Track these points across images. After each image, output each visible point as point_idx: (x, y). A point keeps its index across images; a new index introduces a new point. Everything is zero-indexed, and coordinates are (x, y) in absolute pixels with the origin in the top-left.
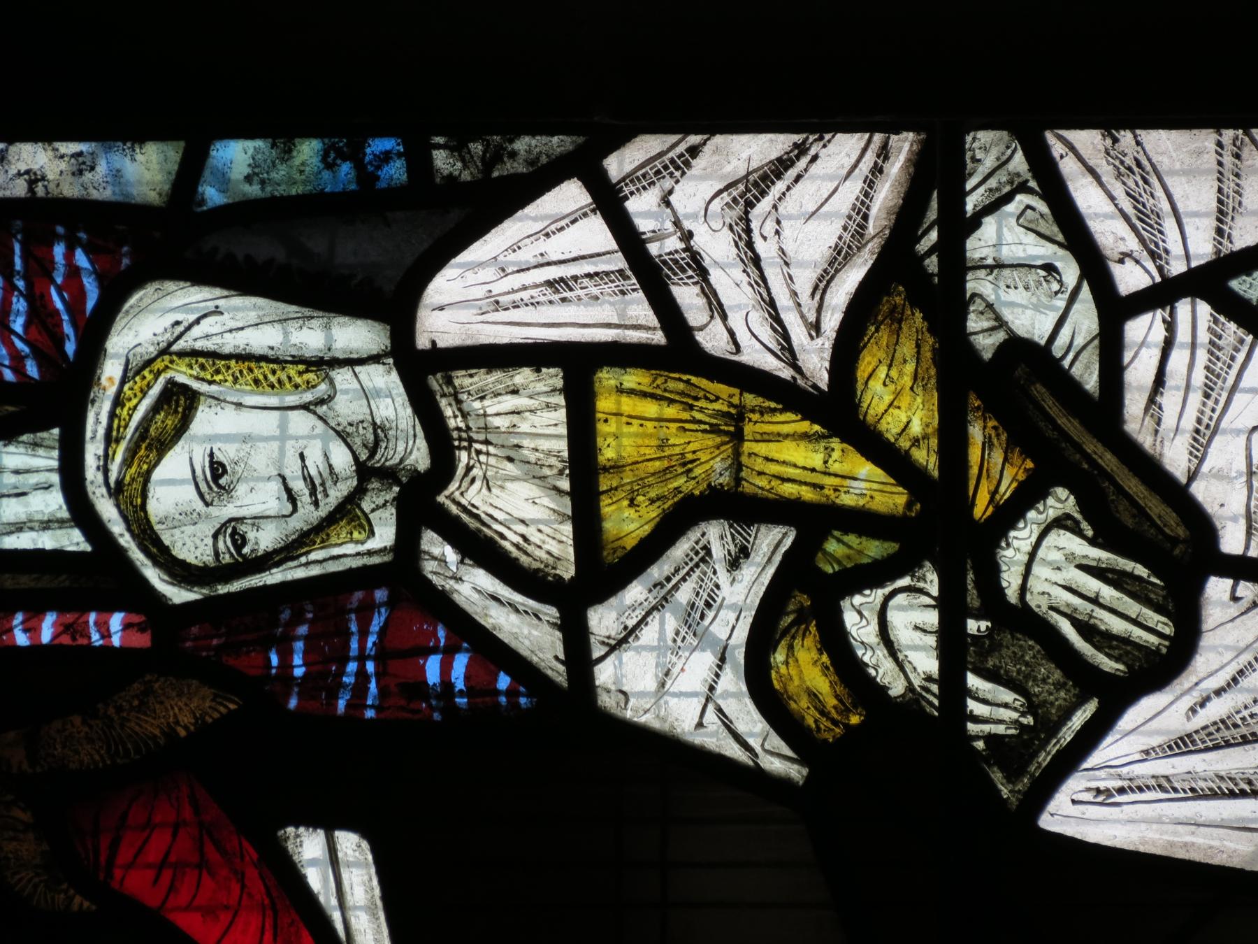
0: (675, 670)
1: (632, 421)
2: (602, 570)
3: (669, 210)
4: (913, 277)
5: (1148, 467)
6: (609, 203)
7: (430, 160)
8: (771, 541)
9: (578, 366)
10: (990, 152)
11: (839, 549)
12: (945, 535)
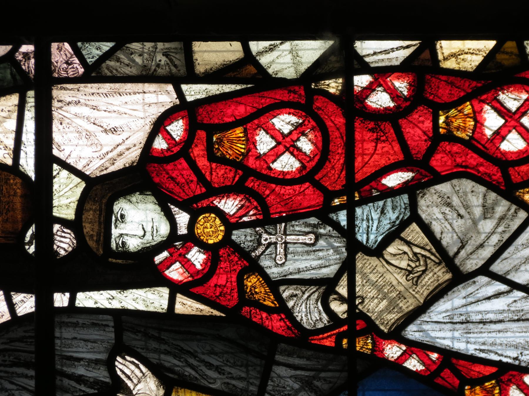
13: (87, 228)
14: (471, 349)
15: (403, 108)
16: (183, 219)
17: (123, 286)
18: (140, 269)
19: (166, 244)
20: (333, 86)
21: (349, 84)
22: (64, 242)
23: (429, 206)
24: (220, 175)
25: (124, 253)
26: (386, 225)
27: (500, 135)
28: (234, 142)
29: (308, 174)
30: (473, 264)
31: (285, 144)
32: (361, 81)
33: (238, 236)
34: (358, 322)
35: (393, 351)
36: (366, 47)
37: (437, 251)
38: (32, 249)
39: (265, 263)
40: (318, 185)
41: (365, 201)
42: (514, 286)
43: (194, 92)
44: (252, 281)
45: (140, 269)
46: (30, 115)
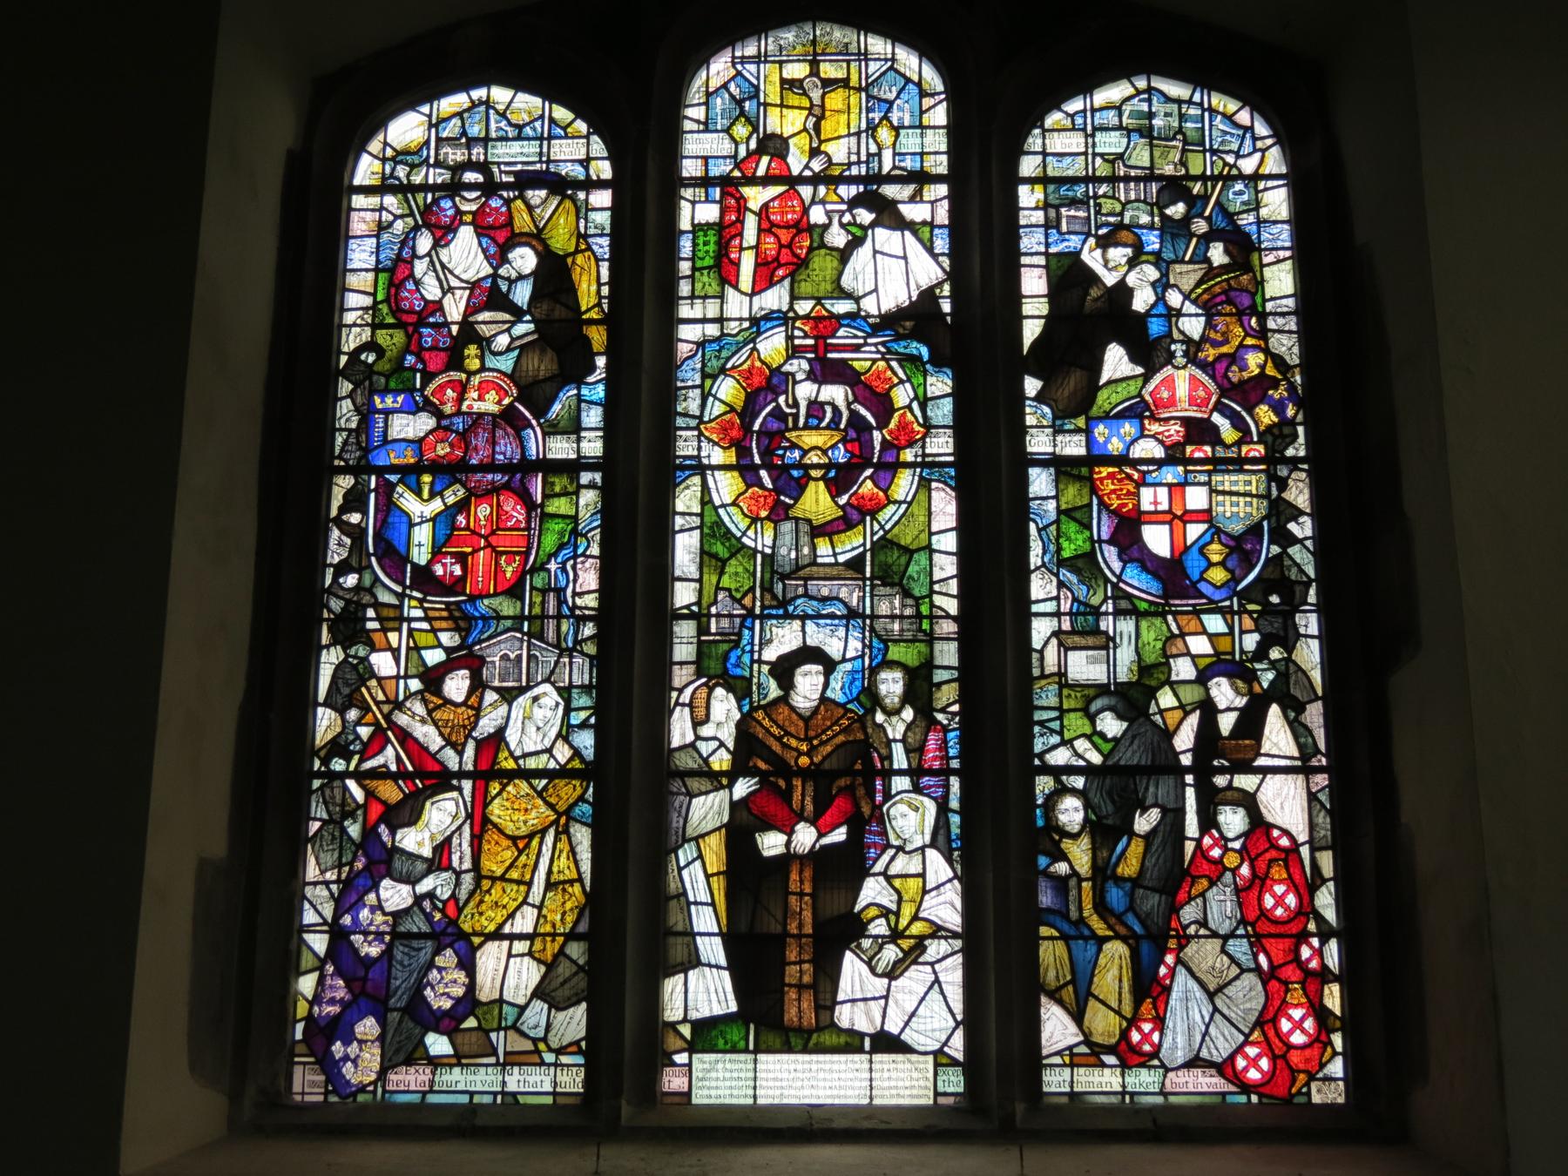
0: (873, 891)
2: (889, 879)
4: (937, 931)
5: (906, 969)
6: (950, 880)
7: (1024, 482)
8: (894, 907)
9: (923, 875)
10: (958, 944)
11: (892, 918)
12: (895, 935)
13: (1229, 793)
14: (1172, 1002)
16: (1237, 845)
18: (1208, 822)
19: (1222, 836)
20: (1312, 927)
21: (1313, 935)
22: (1221, 781)
24: (1261, 865)
25: (1215, 814)
26: (1238, 956)
27: (1290, 1018)
28: (1278, 872)
29: (1264, 914)
30: (1219, 1003)
31: (1280, 901)
32: (1315, 942)
33: (1228, 875)
35: (1170, 959)
36: (1333, 945)
38: (1215, 763)
39: (1215, 889)
40: (1258, 918)
41: (1251, 945)
42: (1207, 1026)
43: (1305, 851)
44: (1205, 883)
45: (1208, 822)
46: (1283, 763)
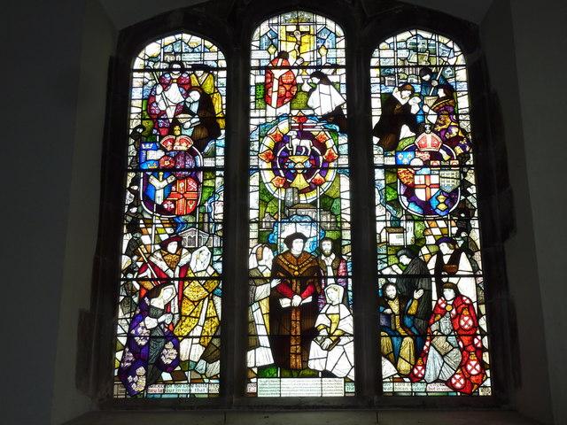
1: (336, 317)
2: (327, 315)
3: (175, 352)
4: (344, 334)
10: (352, 338)
12: (330, 335)
15: (475, 346)
16: (451, 303)
17: (437, 291)
18: (440, 294)
20: (478, 332)
22: (445, 280)
23: (456, 351)
24: (459, 309)
25: (443, 291)
29: (460, 327)
34: (432, 337)
35: (428, 343)
36: (486, 338)
37: (353, 241)
41: (457, 339)
43: (475, 305)
45: (440, 294)
46: (469, 273)
